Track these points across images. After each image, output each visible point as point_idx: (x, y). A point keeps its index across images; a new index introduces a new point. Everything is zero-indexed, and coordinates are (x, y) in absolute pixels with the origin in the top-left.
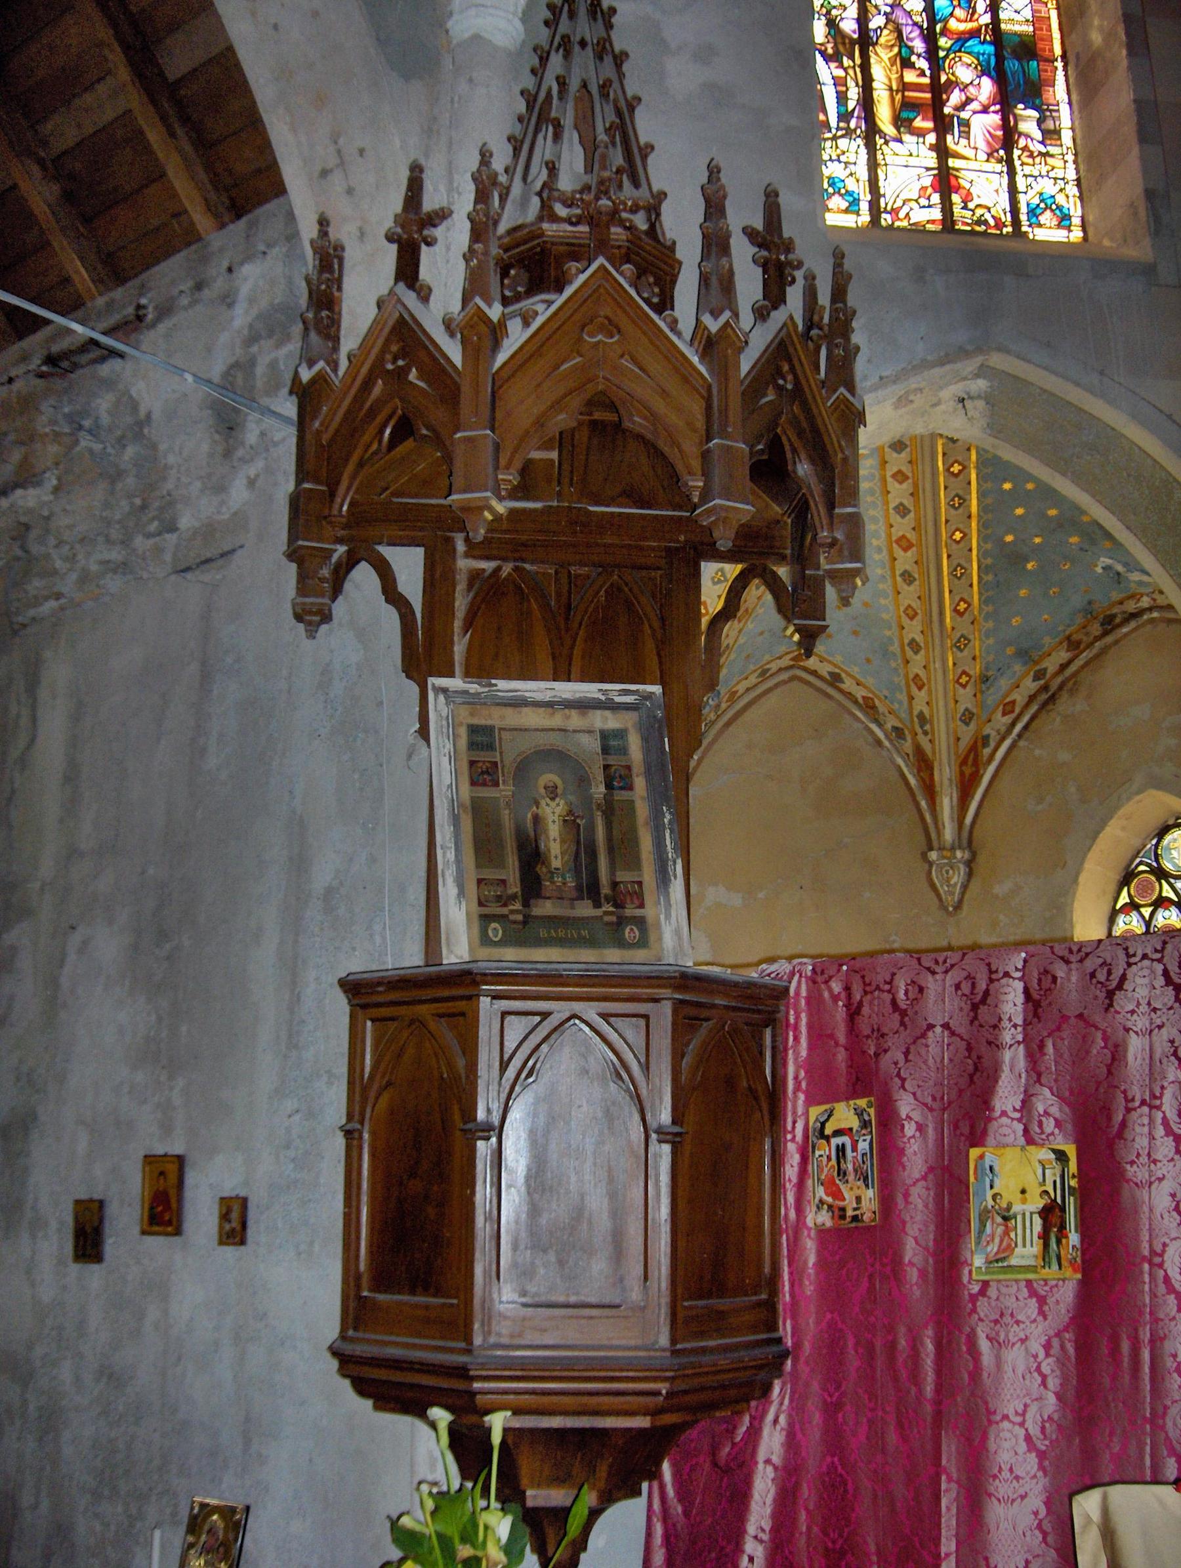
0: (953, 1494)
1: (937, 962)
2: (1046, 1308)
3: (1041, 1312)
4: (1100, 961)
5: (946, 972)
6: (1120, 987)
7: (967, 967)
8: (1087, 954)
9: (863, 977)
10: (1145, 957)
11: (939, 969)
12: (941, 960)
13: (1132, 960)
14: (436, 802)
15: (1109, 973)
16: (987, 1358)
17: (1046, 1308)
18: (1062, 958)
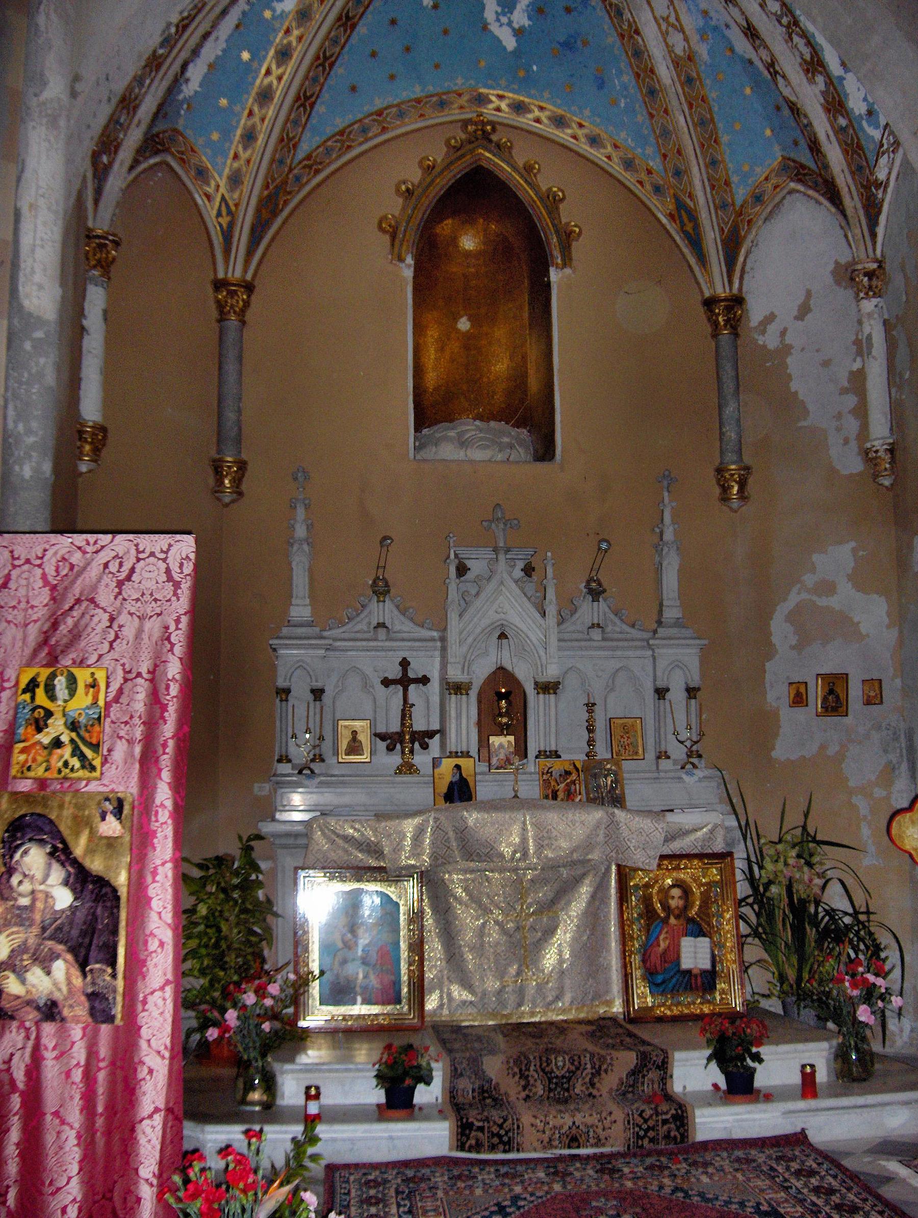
0: (189, 584)
1: (88, 544)
2: (179, 591)
3: (175, 594)
4: (113, 554)
5: (97, 552)
6: (129, 578)
7: (116, 548)
8: (103, 547)
9: (12, 552)
10: (28, 561)
11: (89, 549)
12: (92, 541)
13: (141, 556)
14: (732, 795)
15: (121, 564)
16: (691, 204)
17: (179, 591)
18: (79, 548)
